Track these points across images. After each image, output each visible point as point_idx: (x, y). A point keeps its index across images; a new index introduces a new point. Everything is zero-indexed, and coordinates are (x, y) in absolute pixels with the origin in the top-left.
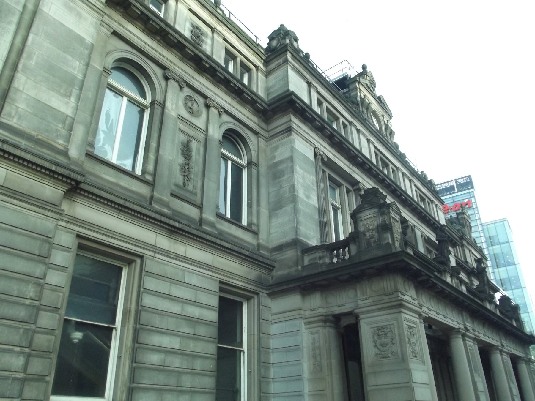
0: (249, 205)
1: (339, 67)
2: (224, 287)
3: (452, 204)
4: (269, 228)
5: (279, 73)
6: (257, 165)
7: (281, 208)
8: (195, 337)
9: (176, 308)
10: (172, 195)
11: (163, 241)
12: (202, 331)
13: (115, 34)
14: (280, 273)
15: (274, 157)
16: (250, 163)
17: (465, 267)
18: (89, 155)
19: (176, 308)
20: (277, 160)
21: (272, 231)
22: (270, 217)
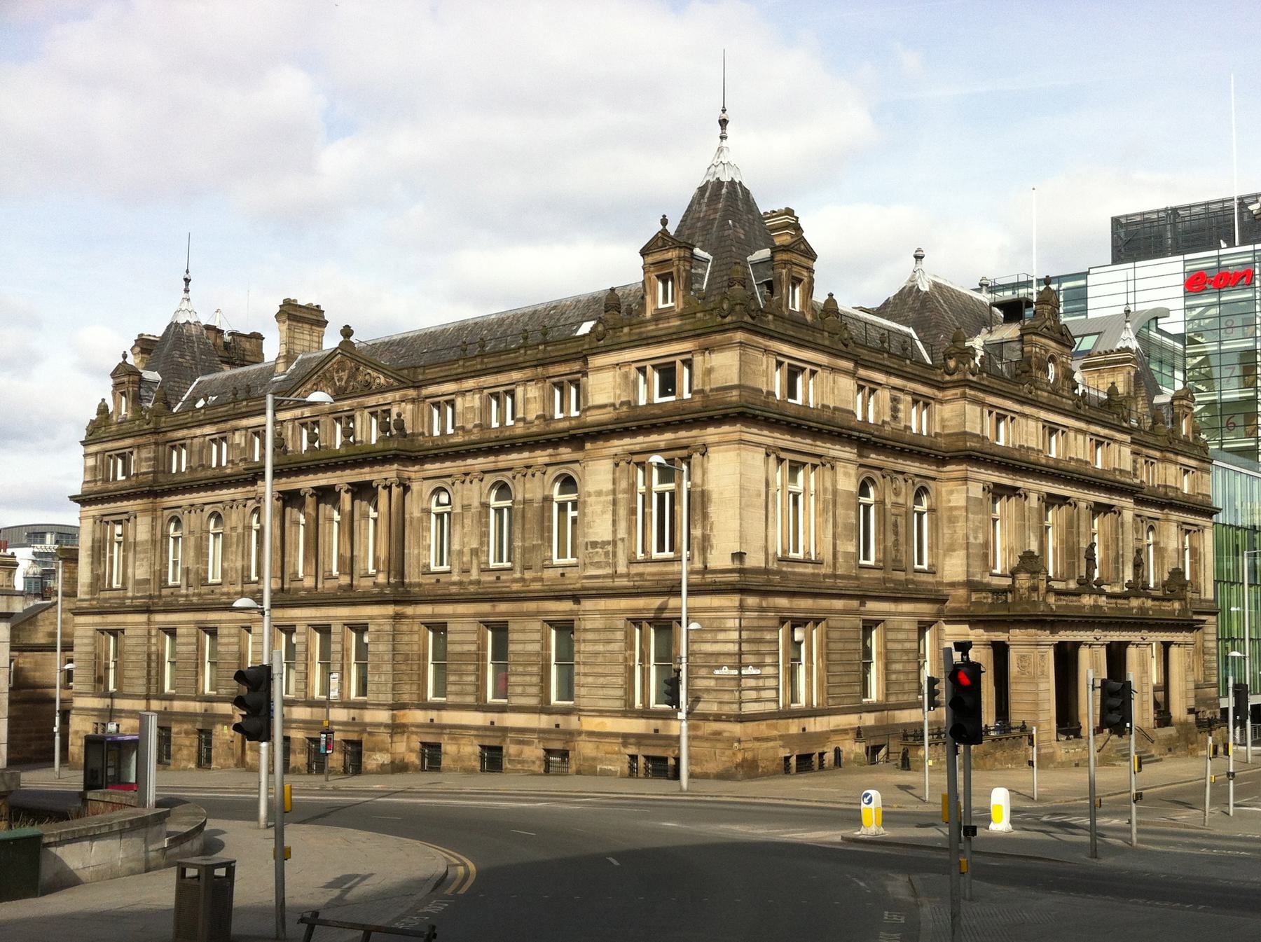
3: (1216, 273)
7: (954, 550)
8: (908, 661)
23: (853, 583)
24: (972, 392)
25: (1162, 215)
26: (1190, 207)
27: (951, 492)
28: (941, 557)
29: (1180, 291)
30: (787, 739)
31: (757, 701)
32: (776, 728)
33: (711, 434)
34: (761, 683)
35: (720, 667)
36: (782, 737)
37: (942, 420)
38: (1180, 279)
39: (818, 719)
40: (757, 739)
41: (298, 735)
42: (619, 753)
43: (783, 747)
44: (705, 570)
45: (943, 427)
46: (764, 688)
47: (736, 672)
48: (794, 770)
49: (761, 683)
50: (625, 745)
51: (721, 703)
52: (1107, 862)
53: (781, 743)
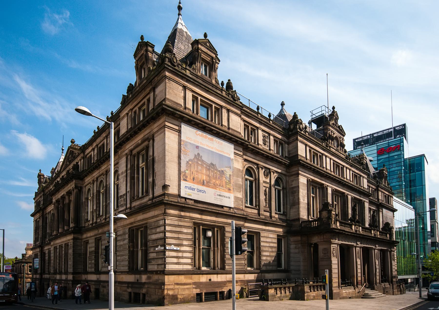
0: (284, 205)
1: (320, 110)
2: (278, 235)
3: (387, 148)
4: (290, 212)
5: (293, 144)
6: (286, 189)
7: (294, 206)
8: (272, 252)
9: (268, 245)
10: (264, 211)
11: (264, 227)
12: (274, 250)
13: (77, 110)
14: (294, 229)
15: (292, 185)
16: (283, 188)
17: (96, 166)
18: (106, 301)
19: (268, 245)
20: (159, 49)
21: (291, 214)
22: (290, 208)
23: (242, 212)
24: (301, 139)
25: (369, 137)
26: (378, 133)
27: (293, 181)
28: (288, 209)
29: (376, 155)
30: (198, 285)
31: (177, 264)
32: (191, 279)
33: (155, 126)
34: (180, 254)
35: (157, 246)
36: (194, 283)
37: (289, 151)
38: (376, 151)
39: (219, 276)
40: (177, 284)
41: (176, 291)
42: (126, 291)
43: (196, 288)
44: (154, 198)
45: (289, 154)
46: (183, 257)
47: (163, 248)
48: (204, 300)
49: (180, 254)
50: (128, 287)
51: (158, 265)
52: (230, 131)
53: (194, 286)
